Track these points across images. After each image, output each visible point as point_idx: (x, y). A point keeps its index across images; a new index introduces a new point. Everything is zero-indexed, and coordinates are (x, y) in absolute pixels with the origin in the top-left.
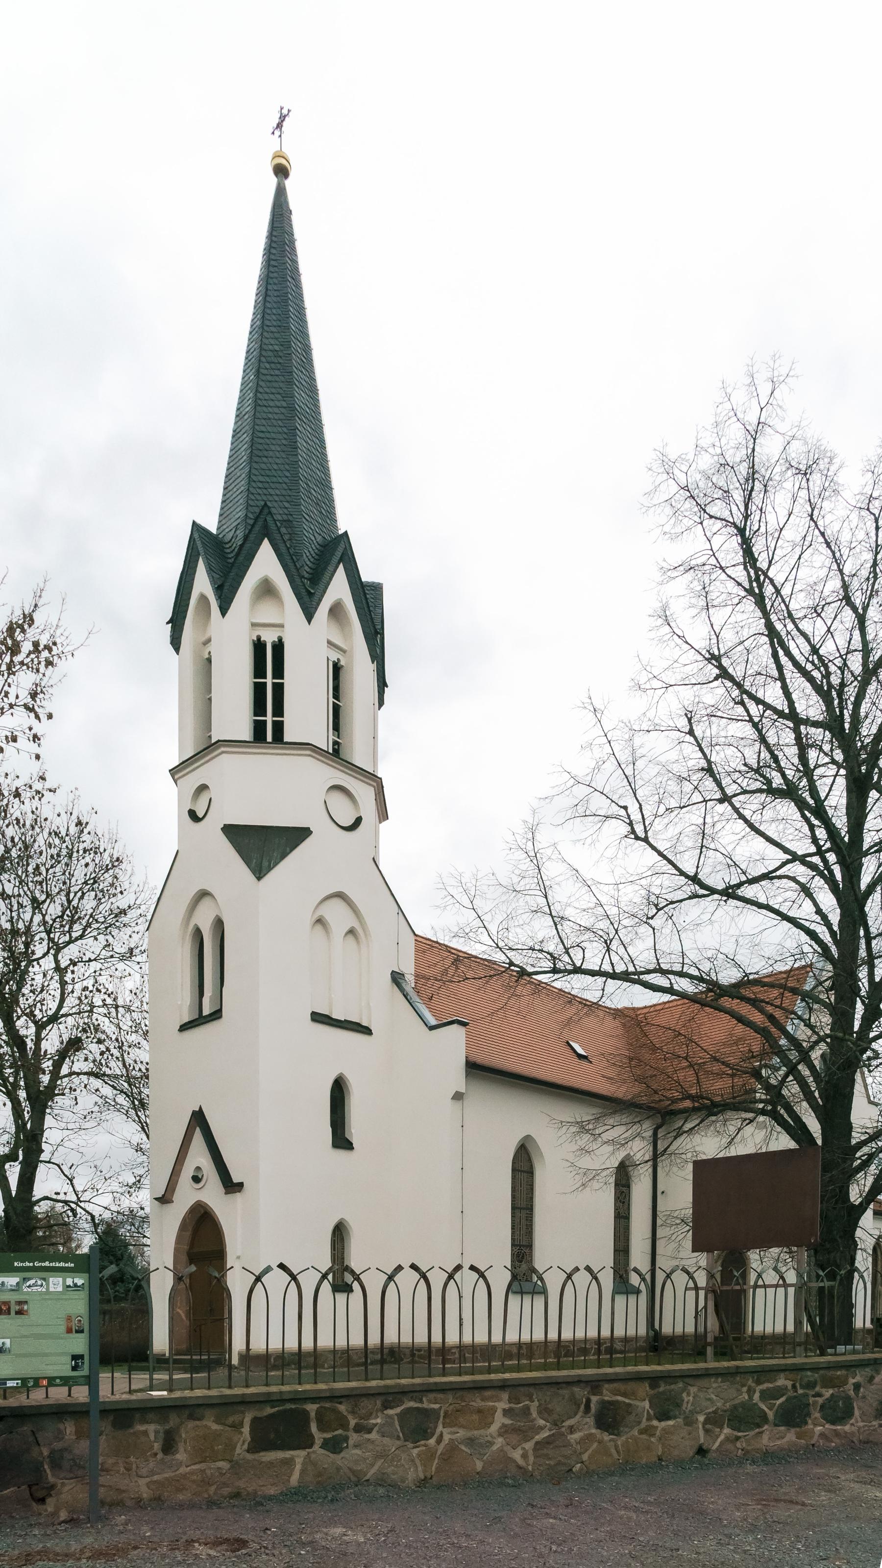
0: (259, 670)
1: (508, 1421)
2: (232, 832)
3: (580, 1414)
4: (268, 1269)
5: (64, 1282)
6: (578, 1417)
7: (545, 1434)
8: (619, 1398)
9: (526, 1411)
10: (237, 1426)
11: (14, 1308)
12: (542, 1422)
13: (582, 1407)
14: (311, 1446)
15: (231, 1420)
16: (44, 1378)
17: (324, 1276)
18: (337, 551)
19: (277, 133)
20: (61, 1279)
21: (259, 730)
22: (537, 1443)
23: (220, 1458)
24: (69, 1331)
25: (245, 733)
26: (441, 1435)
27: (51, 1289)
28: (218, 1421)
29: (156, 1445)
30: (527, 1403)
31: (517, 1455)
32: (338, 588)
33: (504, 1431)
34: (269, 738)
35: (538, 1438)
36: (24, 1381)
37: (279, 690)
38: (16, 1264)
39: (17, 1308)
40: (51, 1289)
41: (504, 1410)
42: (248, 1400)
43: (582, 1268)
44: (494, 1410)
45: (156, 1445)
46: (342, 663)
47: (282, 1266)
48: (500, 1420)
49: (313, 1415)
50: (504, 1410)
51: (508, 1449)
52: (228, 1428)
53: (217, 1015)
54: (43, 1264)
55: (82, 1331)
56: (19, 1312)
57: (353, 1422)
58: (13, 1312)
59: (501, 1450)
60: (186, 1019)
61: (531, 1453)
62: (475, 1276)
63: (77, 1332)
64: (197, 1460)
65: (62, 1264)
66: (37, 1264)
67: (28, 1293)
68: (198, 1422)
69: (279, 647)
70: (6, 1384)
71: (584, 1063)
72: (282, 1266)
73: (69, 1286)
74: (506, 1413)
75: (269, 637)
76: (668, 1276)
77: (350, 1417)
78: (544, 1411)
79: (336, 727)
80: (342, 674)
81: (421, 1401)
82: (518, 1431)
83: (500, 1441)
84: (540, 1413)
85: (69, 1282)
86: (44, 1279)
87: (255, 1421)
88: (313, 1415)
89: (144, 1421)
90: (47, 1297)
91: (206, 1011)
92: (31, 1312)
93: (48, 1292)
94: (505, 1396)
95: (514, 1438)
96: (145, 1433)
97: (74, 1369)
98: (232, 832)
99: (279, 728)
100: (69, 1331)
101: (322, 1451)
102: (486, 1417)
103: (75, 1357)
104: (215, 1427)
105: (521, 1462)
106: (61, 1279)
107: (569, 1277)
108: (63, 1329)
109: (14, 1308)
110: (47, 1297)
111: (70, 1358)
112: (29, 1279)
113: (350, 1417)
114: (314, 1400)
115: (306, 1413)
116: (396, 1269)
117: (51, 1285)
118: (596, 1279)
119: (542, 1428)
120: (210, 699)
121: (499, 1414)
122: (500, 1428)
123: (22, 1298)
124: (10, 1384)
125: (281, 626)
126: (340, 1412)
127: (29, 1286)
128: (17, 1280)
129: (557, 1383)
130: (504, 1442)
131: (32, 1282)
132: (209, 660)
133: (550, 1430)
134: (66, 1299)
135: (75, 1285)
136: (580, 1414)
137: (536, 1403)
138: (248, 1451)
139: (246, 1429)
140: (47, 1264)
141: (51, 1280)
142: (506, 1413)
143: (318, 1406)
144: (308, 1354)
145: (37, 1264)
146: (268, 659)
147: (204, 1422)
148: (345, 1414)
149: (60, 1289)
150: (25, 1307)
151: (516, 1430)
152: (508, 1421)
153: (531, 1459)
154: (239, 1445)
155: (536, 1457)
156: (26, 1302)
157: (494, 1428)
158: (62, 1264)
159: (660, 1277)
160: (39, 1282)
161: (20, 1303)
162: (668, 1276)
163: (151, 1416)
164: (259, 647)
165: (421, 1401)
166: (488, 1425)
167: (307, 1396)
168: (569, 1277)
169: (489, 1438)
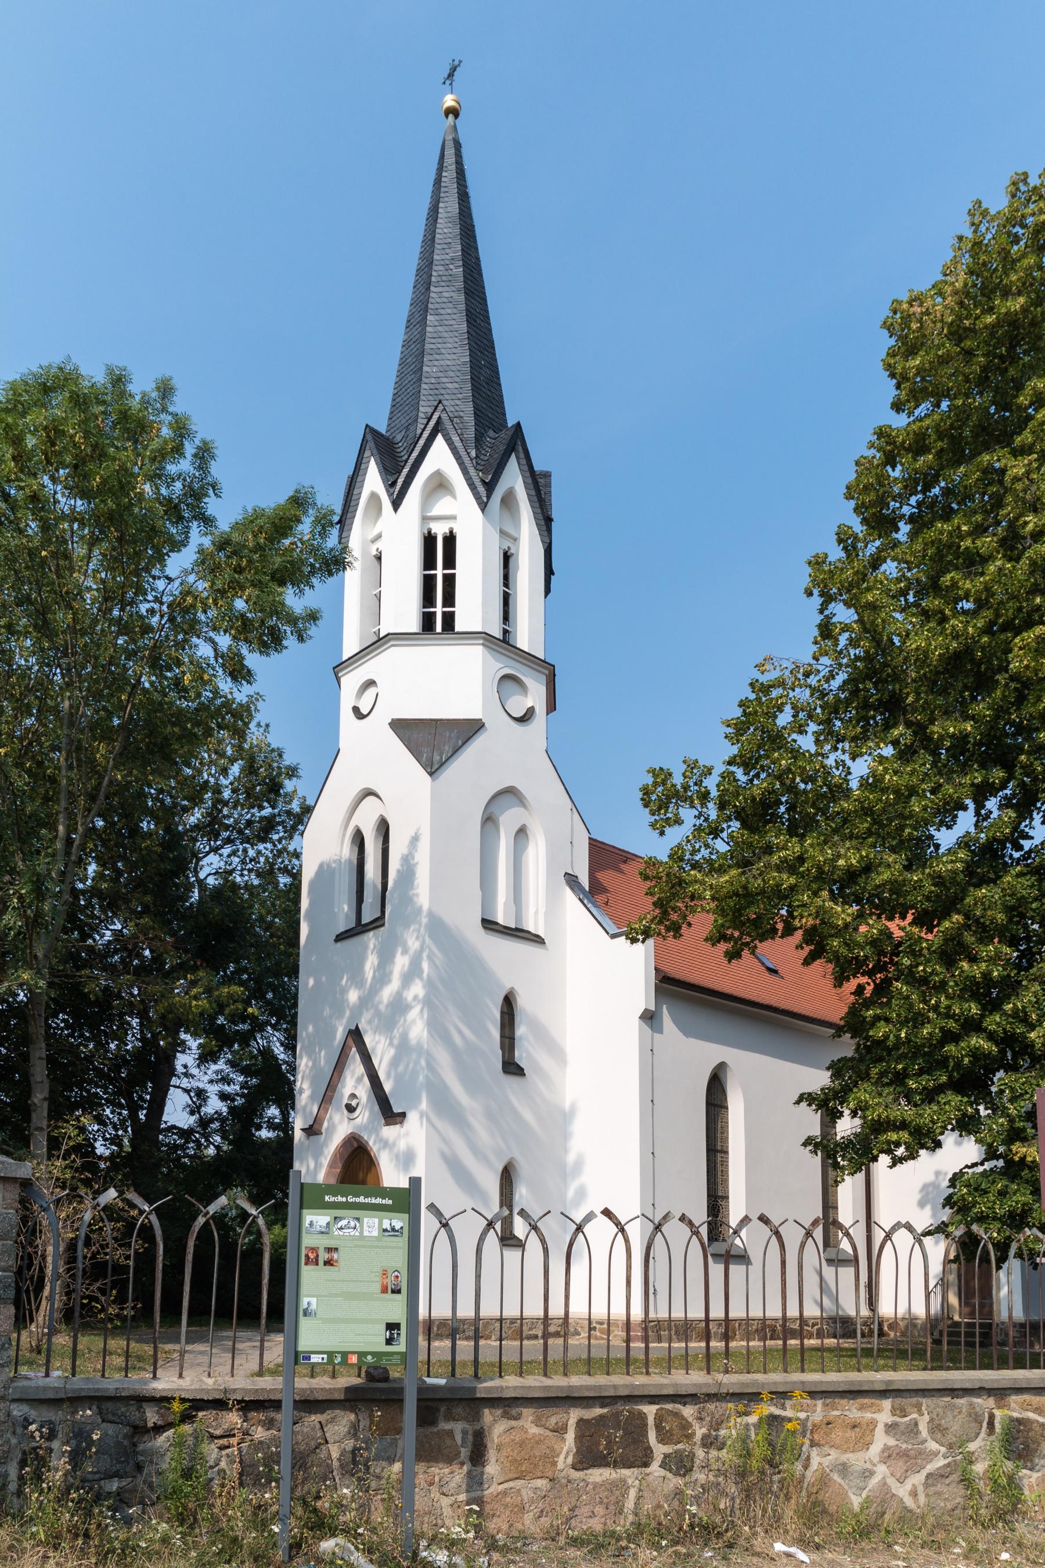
0: (429, 561)
1: (892, 1442)
2: (401, 727)
3: (983, 1435)
4: (590, 1217)
5: (380, 1223)
6: (979, 1439)
7: (940, 1462)
8: (1031, 1415)
9: (913, 1429)
10: (560, 1430)
11: (323, 1256)
12: (933, 1446)
13: (985, 1425)
14: (646, 1465)
15: (553, 1420)
16: (354, 1353)
17: (490, 1225)
18: (516, 441)
19: (448, 82)
20: (376, 1220)
21: (428, 623)
22: (929, 1476)
23: (539, 1474)
24: (384, 1290)
25: (413, 624)
26: (808, 1459)
27: (366, 1233)
28: (537, 1423)
29: (463, 1450)
30: (915, 1416)
31: (903, 1492)
32: (513, 478)
33: (888, 1456)
34: (439, 628)
35: (930, 1468)
36: (331, 1355)
37: (450, 582)
38: (327, 1198)
39: (327, 1256)
40: (366, 1233)
41: (886, 1425)
42: (576, 1395)
43: (598, 1212)
44: (873, 1424)
45: (463, 1450)
46: (512, 551)
47: (607, 1213)
48: (881, 1440)
49: (651, 1421)
50: (886, 1425)
51: (891, 1481)
52: (548, 1433)
53: (378, 923)
54: (358, 1200)
55: (399, 1292)
56: (328, 1263)
57: (700, 1431)
58: (321, 1262)
59: (884, 1483)
60: (342, 929)
61: (920, 1489)
62: (766, 1231)
63: (393, 1292)
64: (511, 1476)
65: (379, 1201)
66: (351, 1199)
67: (339, 1237)
68: (513, 1423)
69: (450, 540)
70: (309, 1358)
71: (773, 978)
72: (607, 1213)
73: (385, 1230)
74: (890, 1428)
75: (440, 530)
76: (888, 1236)
77: (696, 1426)
78: (937, 1429)
79: (506, 618)
80: (511, 561)
81: (783, 1408)
82: (906, 1459)
83: (882, 1470)
84: (932, 1431)
85: (386, 1224)
86: (358, 1219)
87: (581, 1422)
88: (651, 1421)
89: (450, 1417)
90: (360, 1243)
91: (365, 920)
92: (342, 1263)
93: (362, 1237)
94: (887, 1404)
95: (900, 1466)
96: (450, 1433)
97: (389, 1342)
98: (401, 727)
99: (449, 621)
100: (384, 1290)
101: (662, 1472)
102: (862, 1433)
103: (392, 1327)
104: (534, 1430)
105: (909, 1502)
106: (376, 1220)
107: (658, 1228)
108: (377, 1287)
109: (323, 1256)
110: (360, 1243)
111: (384, 1327)
112: (341, 1219)
113: (696, 1426)
114: (653, 1399)
115: (643, 1417)
116: (742, 1221)
117: (365, 1228)
118: (777, 1233)
119: (936, 1454)
120: (379, 597)
121: (880, 1429)
122: (883, 1452)
123: (332, 1244)
124: (315, 1359)
125: (453, 518)
126: (683, 1418)
127: (341, 1229)
128: (327, 1219)
129: (953, 1390)
130: (888, 1473)
131: (343, 1223)
132: (379, 558)
133: (945, 1457)
134: (382, 1247)
135: (393, 1229)
136: (983, 1435)
137: (926, 1418)
138: (574, 1467)
139: (570, 1436)
140: (361, 1199)
141: (366, 1220)
142: (890, 1428)
143: (657, 1407)
144: (513, 1321)
145: (351, 1199)
146: (438, 551)
147: (520, 1423)
148: (690, 1420)
149: (375, 1233)
150: (336, 1256)
151: (905, 1455)
152: (892, 1442)
153: (922, 1499)
154: (562, 1456)
155: (927, 1495)
156: (336, 1249)
157: (876, 1449)
158: (379, 1201)
159: (879, 1236)
160: (352, 1224)
161: (329, 1250)
162: (888, 1236)
163: (459, 1410)
164: (429, 540)
165: (783, 1408)
166: (867, 1445)
167: (646, 1393)
168: (658, 1228)
169: (868, 1466)
